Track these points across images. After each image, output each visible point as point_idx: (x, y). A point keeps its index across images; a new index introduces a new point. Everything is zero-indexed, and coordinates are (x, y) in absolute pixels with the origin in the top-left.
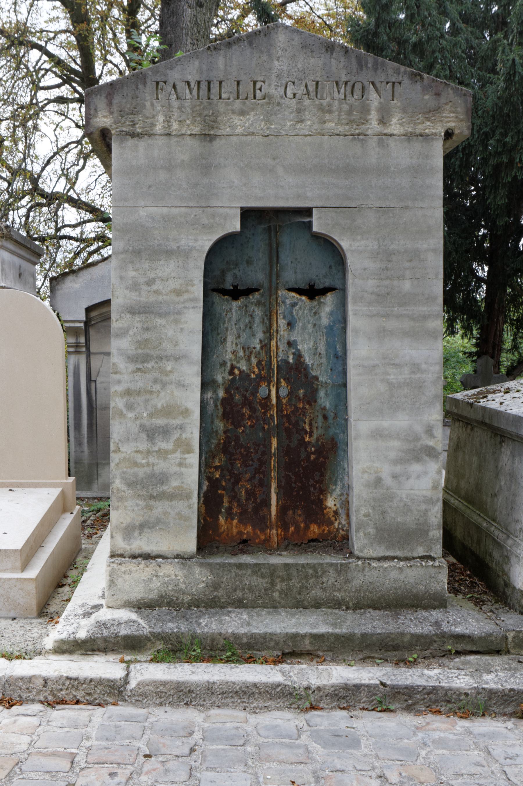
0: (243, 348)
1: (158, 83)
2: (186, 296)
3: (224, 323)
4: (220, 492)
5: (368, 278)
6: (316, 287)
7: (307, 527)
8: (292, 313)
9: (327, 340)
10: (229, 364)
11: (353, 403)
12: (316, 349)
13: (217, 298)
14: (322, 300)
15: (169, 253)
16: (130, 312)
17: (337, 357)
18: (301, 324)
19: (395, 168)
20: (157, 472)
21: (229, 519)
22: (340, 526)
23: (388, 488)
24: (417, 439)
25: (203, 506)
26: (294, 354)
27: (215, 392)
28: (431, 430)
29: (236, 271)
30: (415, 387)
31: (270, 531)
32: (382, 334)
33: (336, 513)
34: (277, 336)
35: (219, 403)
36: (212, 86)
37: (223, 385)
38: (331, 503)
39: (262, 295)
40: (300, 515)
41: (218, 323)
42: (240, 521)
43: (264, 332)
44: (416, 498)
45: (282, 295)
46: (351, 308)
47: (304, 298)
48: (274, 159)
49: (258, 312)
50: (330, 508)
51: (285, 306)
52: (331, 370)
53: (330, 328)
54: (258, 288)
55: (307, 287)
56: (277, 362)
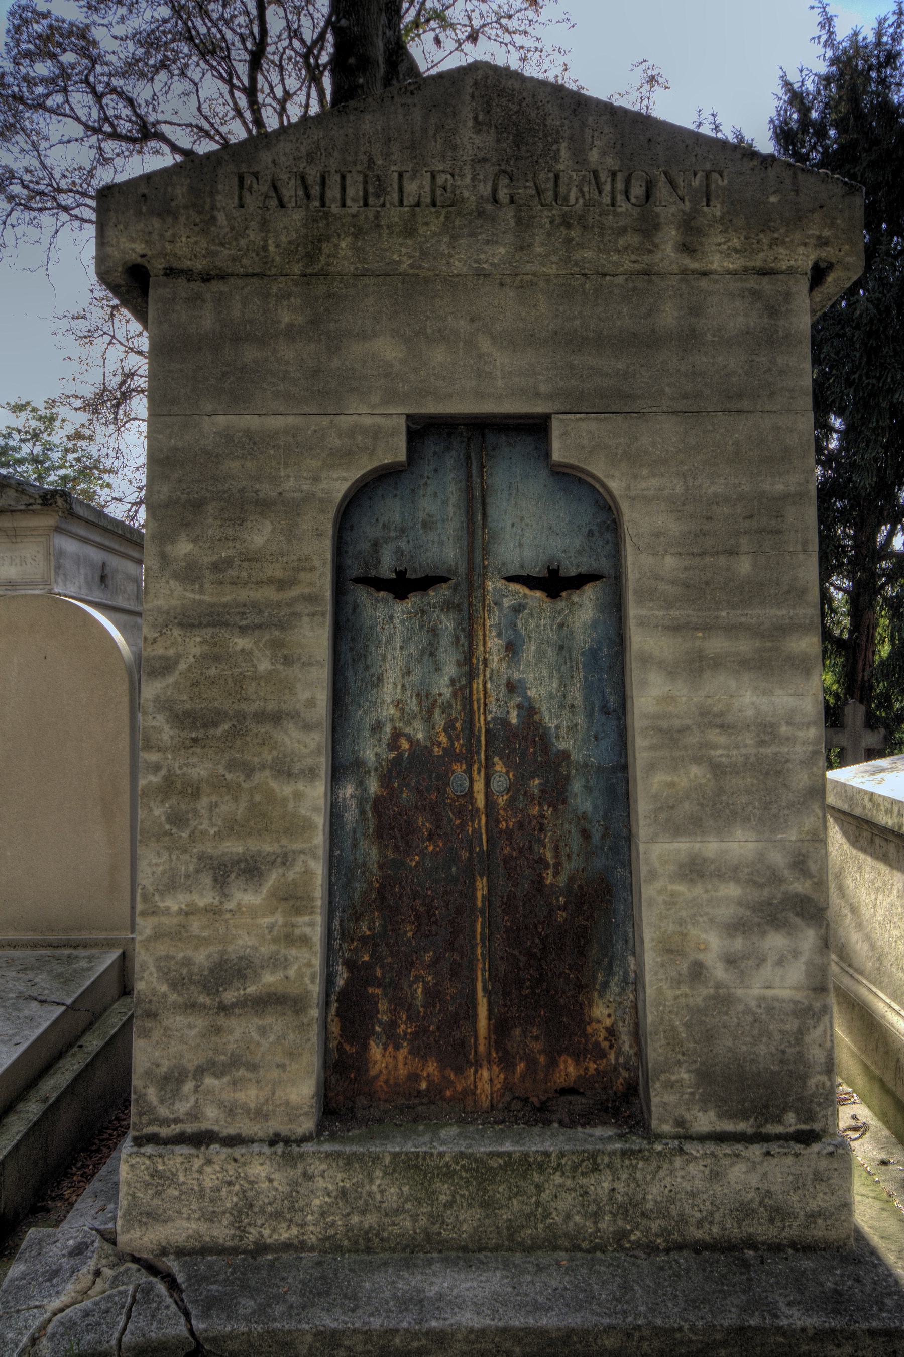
0: (418, 695)
1: (241, 179)
2: (295, 592)
3: (378, 646)
4: (370, 990)
5: (666, 552)
6: (562, 573)
7: (553, 1063)
8: (515, 625)
9: (585, 677)
10: (388, 729)
11: (643, 807)
12: (564, 696)
13: (363, 596)
14: (576, 599)
15: (264, 506)
16: (181, 625)
17: (608, 713)
18: (533, 647)
19: (714, 336)
20: (233, 956)
21: (390, 1048)
22: (621, 1060)
23: (718, 986)
24: (775, 878)
25: (336, 1019)
26: (519, 707)
27: (360, 784)
28: (803, 862)
29: (403, 544)
30: (767, 773)
31: (476, 1072)
32: (696, 666)
33: (611, 1032)
34: (484, 671)
35: (368, 807)
36: (348, 181)
37: (376, 770)
38: (601, 1012)
39: (455, 589)
40: (537, 1039)
41: (366, 646)
42: (414, 1052)
43: (458, 663)
44: (777, 1004)
45: (494, 589)
46: (633, 611)
47: (538, 594)
48: (472, 320)
49: (448, 624)
50: (599, 1022)
51: (501, 611)
52: (596, 738)
53: (593, 654)
54: (446, 575)
55: (545, 573)
56: (487, 723)
